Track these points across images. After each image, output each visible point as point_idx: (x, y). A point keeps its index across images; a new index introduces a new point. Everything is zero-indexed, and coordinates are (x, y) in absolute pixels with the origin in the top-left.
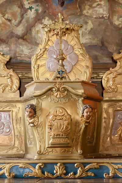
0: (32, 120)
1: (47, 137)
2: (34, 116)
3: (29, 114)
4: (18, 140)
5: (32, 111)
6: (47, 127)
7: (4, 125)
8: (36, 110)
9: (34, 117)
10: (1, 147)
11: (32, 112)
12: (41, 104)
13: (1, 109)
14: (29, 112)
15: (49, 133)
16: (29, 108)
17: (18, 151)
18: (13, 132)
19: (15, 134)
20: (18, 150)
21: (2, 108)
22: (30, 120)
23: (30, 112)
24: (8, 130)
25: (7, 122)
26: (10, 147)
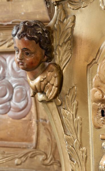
0: (38, 79)
1: (90, 142)
2: (47, 64)
3: (21, 59)
4: (46, 134)
5: (33, 46)
6: (90, 104)
7: (12, 89)
8: (54, 44)
9: (44, 70)
10: (2, 150)
11: (32, 50)
12: (74, 21)
13: (4, 48)
14: (23, 50)
15: (99, 128)
16: (21, 37)
17: (46, 165)
18: (33, 110)
19: (41, 117)
20: (47, 162)
21: (7, 45)
22: (32, 80)
23: (25, 52)
24: (22, 104)
25: (19, 81)
26: (26, 151)
